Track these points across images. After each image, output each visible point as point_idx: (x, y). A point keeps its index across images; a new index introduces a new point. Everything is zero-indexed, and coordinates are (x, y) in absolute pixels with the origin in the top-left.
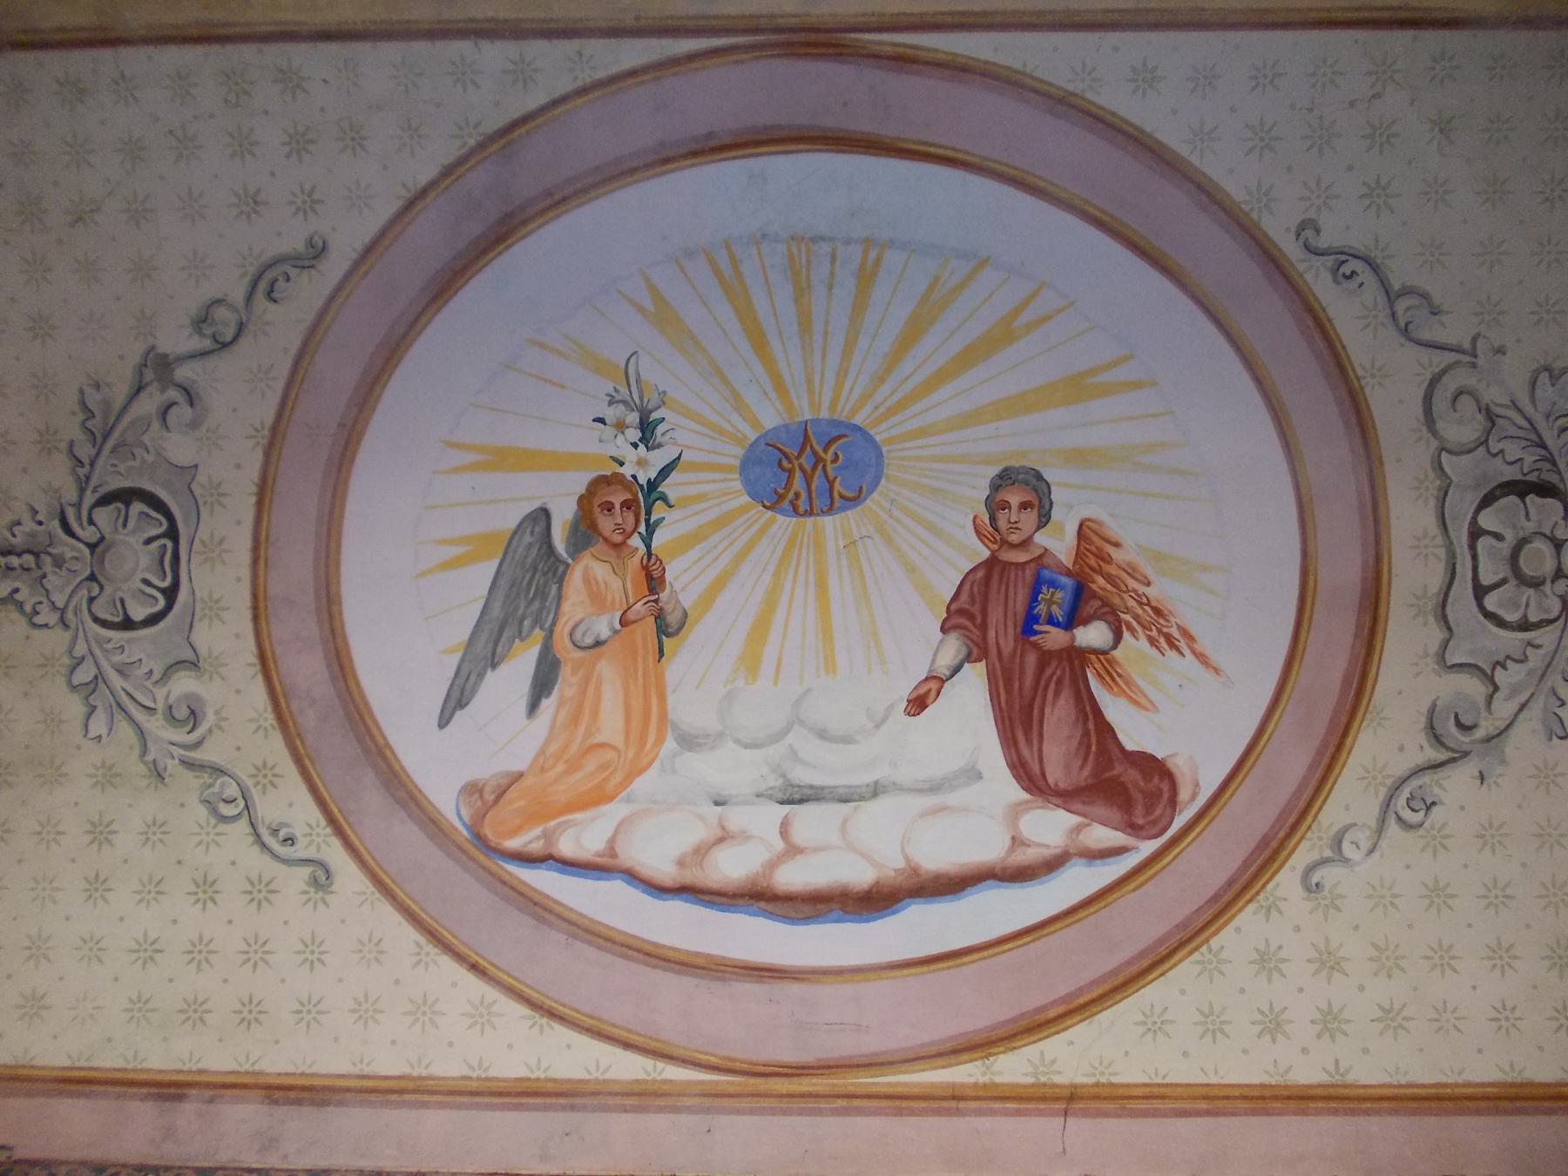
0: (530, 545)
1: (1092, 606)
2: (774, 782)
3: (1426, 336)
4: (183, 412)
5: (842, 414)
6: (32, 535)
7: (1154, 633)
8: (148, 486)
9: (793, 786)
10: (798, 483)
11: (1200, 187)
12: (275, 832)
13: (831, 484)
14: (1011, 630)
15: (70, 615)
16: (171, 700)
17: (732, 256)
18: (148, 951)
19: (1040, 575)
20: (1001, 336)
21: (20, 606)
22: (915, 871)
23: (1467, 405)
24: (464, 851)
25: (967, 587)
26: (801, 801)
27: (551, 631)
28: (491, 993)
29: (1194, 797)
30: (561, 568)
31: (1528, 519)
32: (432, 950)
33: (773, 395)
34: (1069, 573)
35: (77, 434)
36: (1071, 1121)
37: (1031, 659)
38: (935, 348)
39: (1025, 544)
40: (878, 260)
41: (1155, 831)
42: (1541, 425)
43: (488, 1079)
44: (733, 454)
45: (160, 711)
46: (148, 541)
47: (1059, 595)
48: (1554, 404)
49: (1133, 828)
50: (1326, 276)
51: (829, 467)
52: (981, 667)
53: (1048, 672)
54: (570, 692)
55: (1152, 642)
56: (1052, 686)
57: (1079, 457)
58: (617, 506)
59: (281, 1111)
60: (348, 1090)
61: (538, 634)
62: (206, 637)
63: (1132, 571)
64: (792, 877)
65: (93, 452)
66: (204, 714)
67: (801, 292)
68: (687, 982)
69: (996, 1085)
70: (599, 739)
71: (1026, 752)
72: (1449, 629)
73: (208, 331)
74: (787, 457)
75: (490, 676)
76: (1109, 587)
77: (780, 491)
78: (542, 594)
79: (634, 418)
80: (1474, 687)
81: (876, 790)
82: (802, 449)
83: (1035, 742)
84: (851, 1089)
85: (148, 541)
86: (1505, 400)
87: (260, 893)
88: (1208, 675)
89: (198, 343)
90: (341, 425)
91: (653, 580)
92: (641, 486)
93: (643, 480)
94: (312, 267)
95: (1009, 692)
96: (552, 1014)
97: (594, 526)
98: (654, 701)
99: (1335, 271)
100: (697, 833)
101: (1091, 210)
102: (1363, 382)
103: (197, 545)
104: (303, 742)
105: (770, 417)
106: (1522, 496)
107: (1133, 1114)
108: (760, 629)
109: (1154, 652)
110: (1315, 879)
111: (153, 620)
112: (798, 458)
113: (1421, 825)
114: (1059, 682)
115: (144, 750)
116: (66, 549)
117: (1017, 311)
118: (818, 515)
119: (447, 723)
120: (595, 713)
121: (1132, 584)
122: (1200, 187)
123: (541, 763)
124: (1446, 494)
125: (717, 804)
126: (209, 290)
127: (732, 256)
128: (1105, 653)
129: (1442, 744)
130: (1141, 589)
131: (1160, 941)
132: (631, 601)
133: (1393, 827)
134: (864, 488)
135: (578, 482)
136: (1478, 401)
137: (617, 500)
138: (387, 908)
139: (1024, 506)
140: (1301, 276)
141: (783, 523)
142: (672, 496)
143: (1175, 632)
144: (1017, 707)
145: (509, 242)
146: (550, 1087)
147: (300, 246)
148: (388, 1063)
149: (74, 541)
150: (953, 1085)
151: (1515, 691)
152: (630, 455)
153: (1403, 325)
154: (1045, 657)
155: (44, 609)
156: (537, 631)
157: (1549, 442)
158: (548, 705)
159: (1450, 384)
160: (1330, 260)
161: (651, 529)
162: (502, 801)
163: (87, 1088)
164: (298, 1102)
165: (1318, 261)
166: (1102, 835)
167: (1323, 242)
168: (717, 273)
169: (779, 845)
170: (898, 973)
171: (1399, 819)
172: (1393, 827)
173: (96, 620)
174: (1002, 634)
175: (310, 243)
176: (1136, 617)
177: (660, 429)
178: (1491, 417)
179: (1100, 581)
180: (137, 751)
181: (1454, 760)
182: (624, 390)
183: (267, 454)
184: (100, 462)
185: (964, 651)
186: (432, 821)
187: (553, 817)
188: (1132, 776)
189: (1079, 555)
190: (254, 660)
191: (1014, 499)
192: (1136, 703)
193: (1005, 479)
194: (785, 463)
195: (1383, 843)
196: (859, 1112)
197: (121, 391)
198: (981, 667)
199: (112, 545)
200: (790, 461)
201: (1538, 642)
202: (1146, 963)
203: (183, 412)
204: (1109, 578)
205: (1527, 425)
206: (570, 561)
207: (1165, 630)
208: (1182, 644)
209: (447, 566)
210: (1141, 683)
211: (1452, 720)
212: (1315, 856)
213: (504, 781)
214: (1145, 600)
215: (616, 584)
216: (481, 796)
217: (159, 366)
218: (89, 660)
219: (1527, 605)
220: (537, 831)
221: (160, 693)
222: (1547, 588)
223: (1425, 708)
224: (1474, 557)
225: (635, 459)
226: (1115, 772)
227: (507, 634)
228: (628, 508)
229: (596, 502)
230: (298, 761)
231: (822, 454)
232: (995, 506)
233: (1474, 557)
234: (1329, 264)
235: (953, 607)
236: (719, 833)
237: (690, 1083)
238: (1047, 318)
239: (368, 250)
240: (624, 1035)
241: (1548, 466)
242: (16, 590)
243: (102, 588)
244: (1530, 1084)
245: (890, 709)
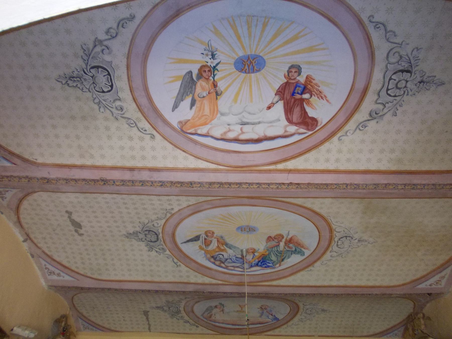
0: (188, 78)
1: (307, 91)
2: (239, 121)
3: (391, 40)
4: (106, 51)
5: (257, 53)
6: (78, 74)
7: (319, 96)
8: (102, 65)
9: (243, 122)
10: (246, 67)
11: (348, 7)
12: (142, 129)
13: (254, 67)
14: (289, 95)
15: (90, 90)
16: (116, 106)
17: (233, 20)
18: (122, 148)
19: (297, 85)
20: (295, 38)
21: (79, 88)
22: (266, 136)
23: (397, 55)
24: (179, 132)
25: (281, 87)
26: (244, 125)
27: (194, 94)
28: (187, 155)
29: (321, 124)
30: (195, 83)
31: (402, 76)
32: (176, 149)
33: (242, 49)
34: (303, 85)
35: (83, 54)
36: (290, 174)
37: (293, 100)
38: (279, 40)
39: (294, 79)
40: (268, 21)
41: (312, 130)
42: (411, 58)
43: (188, 168)
44: (232, 61)
45: (114, 108)
46: (104, 76)
47: (300, 89)
48: (416, 55)
49: (308, 130)
50: (373, 27)
51: (254, 64)
52: (282, 102)
53: (296, 102)
54: (198, 105)
55: (318, 97)
56: (296, 105)
57: (309, 63)
58: (207, 71)
59: (152, 172)
60: (164, 169)
61: (191, 95)
62: (121, 95)
63: (316, 84)
64: (243, 137)
65: (87, 58)
66: (124, 109)
67: (249, 28)
68: (223, 154)
69: (277, 169)
70: (204, 114)
71: (289, 117)
72: (379, 96)
73: (109, 34)
74: (244, 61)
75: (182, 102)
76: (311, 87)
77: (243, 68)
78: (192, 88)
79: (210, 53)
80: (381, 107)
81: (259, 123)
82: (248, 60)
83: (292, 114)
84: (252, 170)
85: (104, 76)
86: (405, 54)
87: (142, 139)
88: (328, 104)
89: (107, 37)
90: (143, 54)
91: (215, 85)
92: (212, 68)
93: (212, 66)
94: (132, 20)
95: (287, 106)
96: (198, 158)
97: (202, 75)
98: (216, 107)
99: (375, 27)
100: (225, 130)
101: (320, 11)
102: (375, 49)
103: (115, 77)
104: (145, 114)
105: (241, 54)
106: (402, 72)
107: (300, 173)
108: (238, 94)
109: (318, 99)
110: (341, 138)
111: (109, 91)
112: (247, 62)
113: (363, 130)
114: (298, 105)
115: (113, 115)
116: (86, 77)
117: (300, 32)
118: (250, 73)
119: (174, 111)
120: (204, 109)
121: (316, 87)
122: (348, 7)
123: (193, 118)
124: (387, 71)
125: (228, 125)
126: (108, 26)
127: (233, 20)
128: (308, 99)
129: (371, 116)
130: (318, 88)
131: (310, 147)
132: (210, 89)
133: (358, 130)
134: (261, 68)
135: (198, 66)
136: (399, 54)
137: (207, 70)
138: (166, 142)
139: (295, 72)
140: (367, 27)
141: (243, 75)
142: (219, 69)
143: (323, 96)
144: (289, 109)
145: (179, 16)
146: (199, 169)
147: (128, 16)
148: (170, 165)
149: (87, 76)
150: (270, 169)
151: (389, 107)
152: (209, 61)
153: (387, 38)
154: (296, 100)
155: (84, 88)
156: (191, 94)
157: (412, 63)
158: (194, 108)
159: (394, 51)
160: (374, 24)
161: (214, 76)
162: (186, 124)
163: (116, 169)
164: (155, 171)
165: (371, 24)
166: (302, 130)
167: (374, 20)
168: (230, 23)
169: (240, 132)
170: (261, 152)
171: (359, 129)
172: (358, 130)
173: (96, 91)
174: (287, 95)
175: (131, 15)
176: (316, 93)
177: (216, 56)
178: (401, 57)
179: (309, 86)
180: (111, 114)
181: (373, 119)
182: (208, 48)
183: (128, 58)
184: (89, 60)
185: (279, 99)
186: (173, 128)
187: (196, 127)
188: (310, 121)
189: (306, 81)
190: (132, 99)
191: (293, 70)
192: (312, 108)
193: (292, 67)
194: (244, 63)
195: (355, 133)
196: (253, 173)
197: (91, 47)
198: (282, 102)
199: (96, 77)
200: (245, 62)
201: (397, 99)
202: (306, 151)
203: (106, 51)
204: (311, 86)
205: (408, 59)
206: (197, 81)
207: (321, 95)
208: (324, 98)
209: (170, 82)
210: (314, 104)
211: (375, 112)
212: (342, 135)
213: (186, 121)
214: (318, 90)
215: (207, 86)
216: (182, 124)
217: (98, 42)
218: (97, 98)
219: (397, 92)
220: (193, 129)
221: (114, 105)
222: (402, 90)
223: (370, 110)
224: (389, 84)
225: (210, 62)
226: (307, 120)
227: (185, 95)
228: (209, 71)
229: (202, 70)
230: (145, 117)
231: (252, 61)
232: (289, 72)
233: (389, 84)
234: (374, 25)
235: (278, 91)
236: (229, 130)
237: (224, 169)
238: (306, 35)
239: (145, 17)
240: (212, 161)
241: (410, 67)
242: (77, 85)
243: (96, 85)
244: (370, 170)
245: (263, 109)
